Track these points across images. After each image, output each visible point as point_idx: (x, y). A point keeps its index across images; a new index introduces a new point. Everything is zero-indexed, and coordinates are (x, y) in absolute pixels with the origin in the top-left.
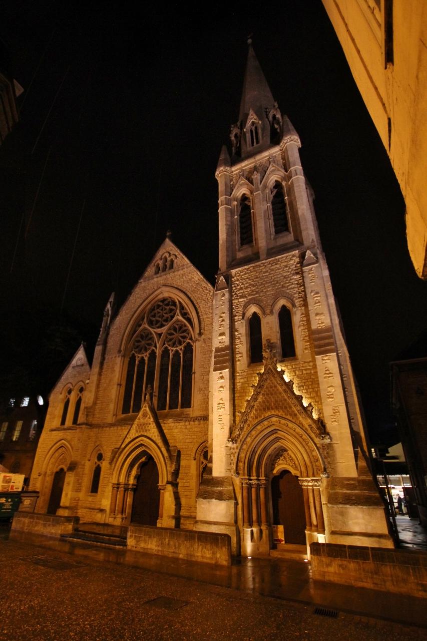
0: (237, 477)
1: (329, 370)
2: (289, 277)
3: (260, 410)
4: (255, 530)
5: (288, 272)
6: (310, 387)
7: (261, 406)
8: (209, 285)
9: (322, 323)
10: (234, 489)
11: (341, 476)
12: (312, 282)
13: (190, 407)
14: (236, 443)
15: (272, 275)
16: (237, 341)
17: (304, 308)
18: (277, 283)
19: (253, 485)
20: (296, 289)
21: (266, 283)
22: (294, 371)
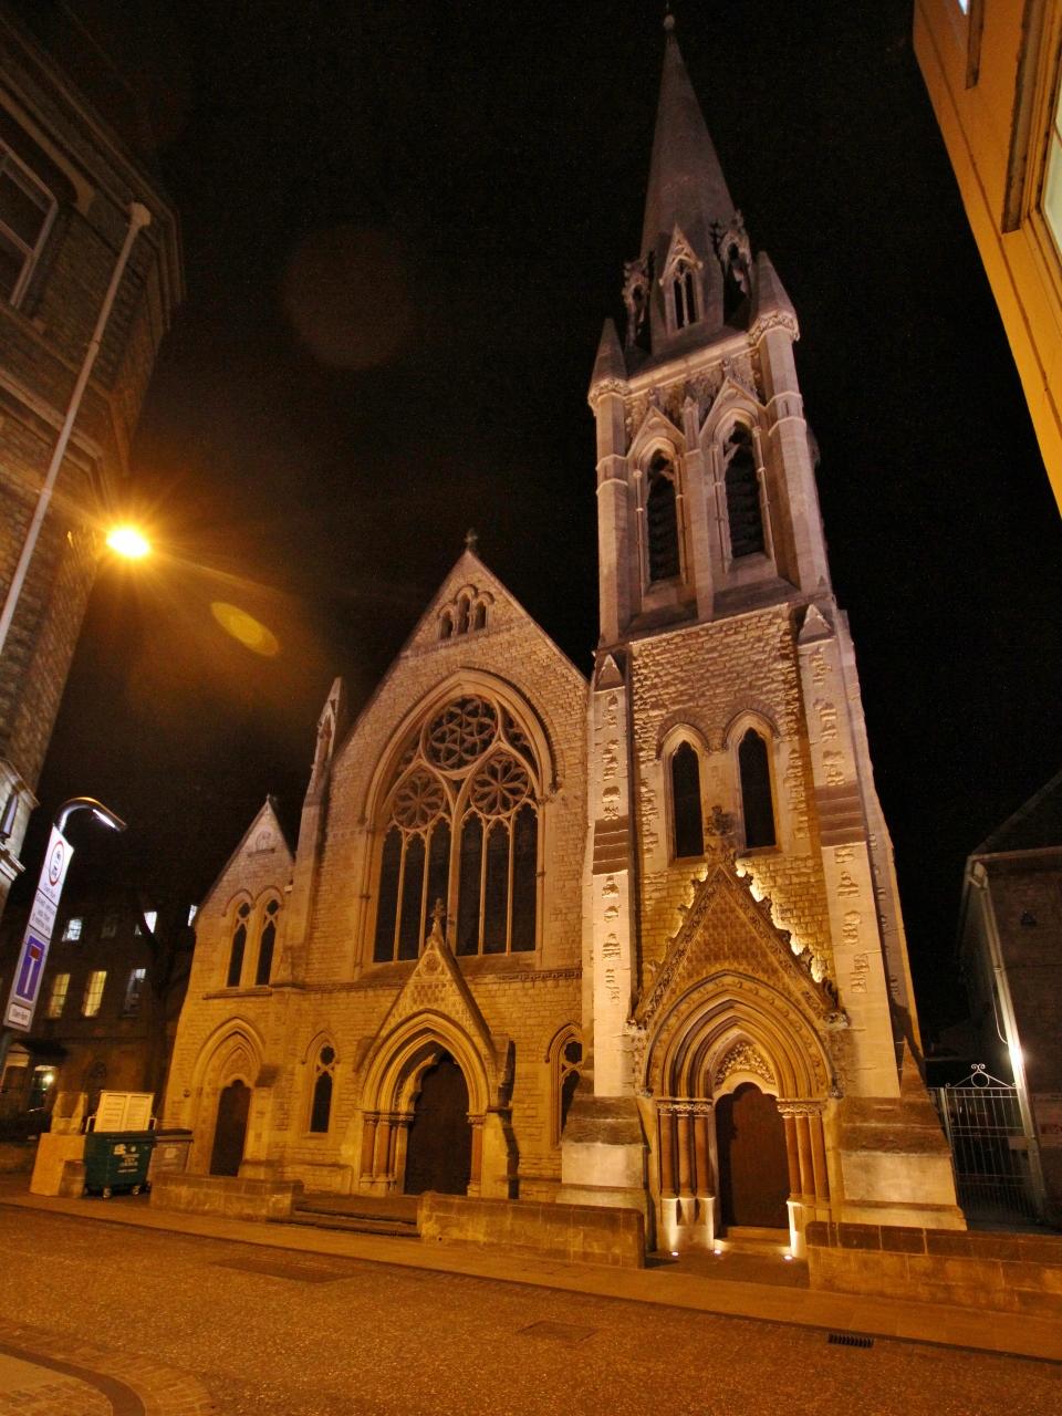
0: (648, 1097)
2: (764, 665)
4: (684, 1201)
5: (764, 652)
6: (807, 912)
7: (701, 952)
9: (839, 774)
10: (642, 1122)
11: (867, 1096)
12: (818, 681)
16: (645, 808)
17: (797, 738)
18: (738, 677)
19: (680, 1112)
20: (781, 694)
21: (714, 676)
22: (771, 877)
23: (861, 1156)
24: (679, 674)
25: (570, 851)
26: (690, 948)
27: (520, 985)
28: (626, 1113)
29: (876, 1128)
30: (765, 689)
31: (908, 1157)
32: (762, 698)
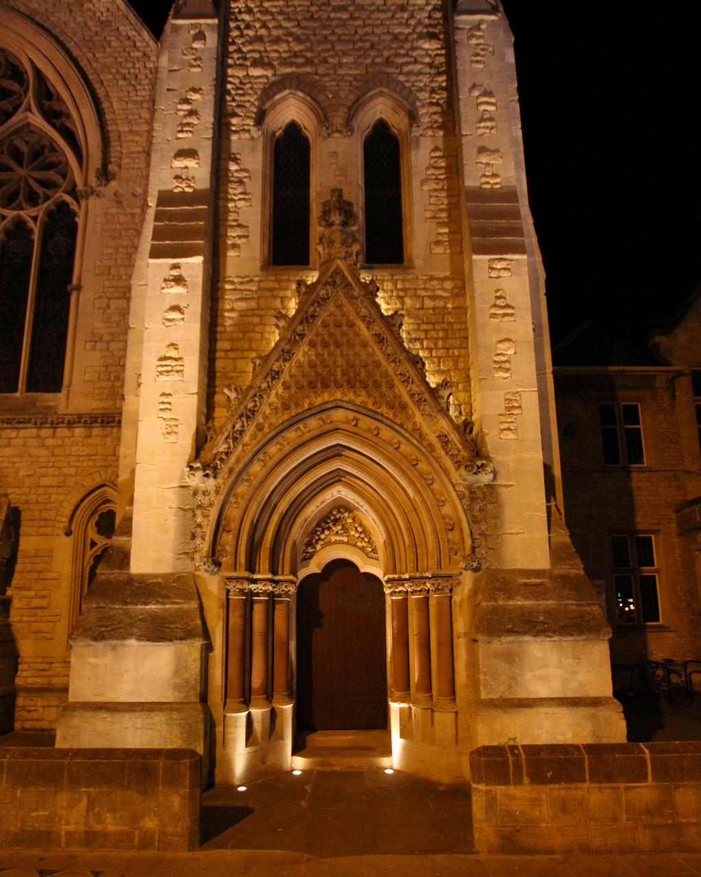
0: (213, 573)
1: (504, 298)
2: (406, 40)
3: (300, 388)
4: (257, 712)
5: (407, 25)
6: (440, 343)
7: (304, 375)
8: (146, 35)
9: (495, 175)
10: (201, 608)
11: (511, 567)
12: (477, 62)
13: (57, 389)
14: (215, 477)
15: (360, 23)
16: (234, 191)
17: (441, 133)
18: (372, 47)
19: (258, 594)
20: (426, 79)
21: (340, 39)
22: (399, 297)
23: (505, 642)
24: (294, 30)
25: (119, 262)
26: (288, 370)
27: (34, 431)
28: (179, 596)
29: (521, 607)
30: (406, 69)
31: (560, 640)
32: (402, 78)
